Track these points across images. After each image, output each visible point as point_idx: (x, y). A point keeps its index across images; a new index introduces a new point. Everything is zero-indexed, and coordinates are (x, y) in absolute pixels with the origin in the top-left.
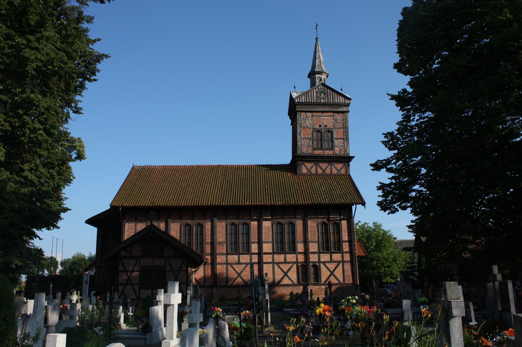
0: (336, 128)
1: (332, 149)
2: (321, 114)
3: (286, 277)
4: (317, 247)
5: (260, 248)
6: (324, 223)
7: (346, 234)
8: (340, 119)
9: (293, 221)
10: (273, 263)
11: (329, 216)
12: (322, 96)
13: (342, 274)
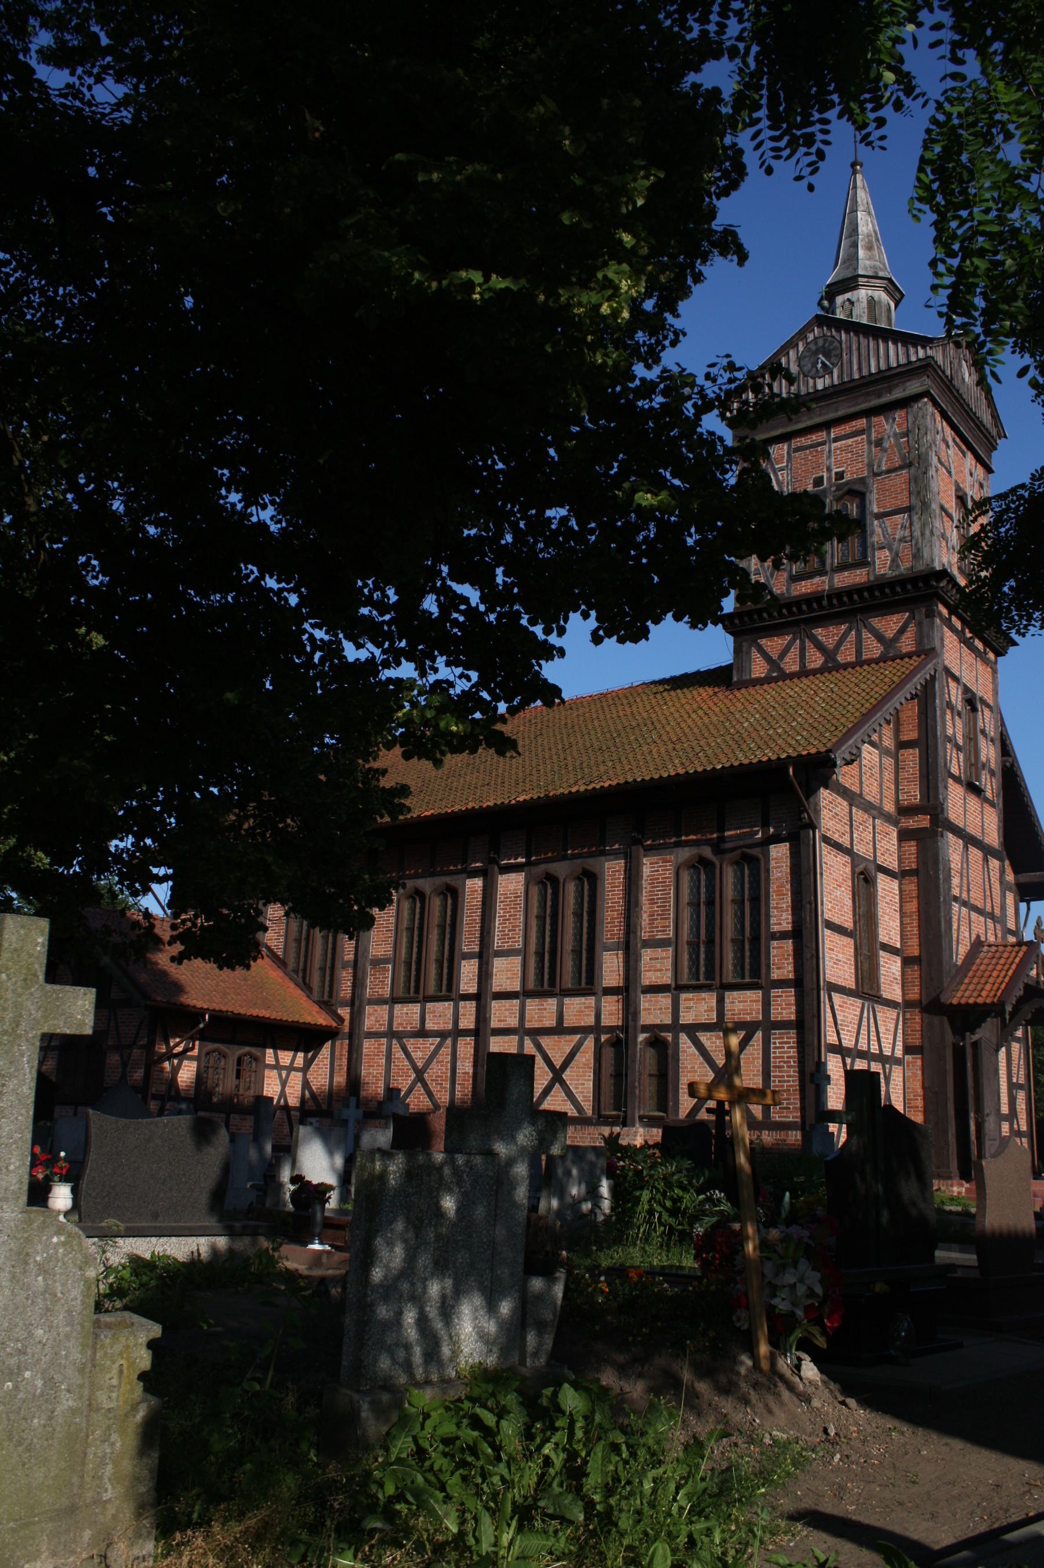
0: (879, 474)
1: (863, 562)
2: (822, 436)
3: (557, 1085)
4: (668, 964)
5: (484, 975)
6: (703, 861)
7: (787, 902)
9: (591, 863)
10: (391, 1034)
11: (724, 832)
12: (819, 365)
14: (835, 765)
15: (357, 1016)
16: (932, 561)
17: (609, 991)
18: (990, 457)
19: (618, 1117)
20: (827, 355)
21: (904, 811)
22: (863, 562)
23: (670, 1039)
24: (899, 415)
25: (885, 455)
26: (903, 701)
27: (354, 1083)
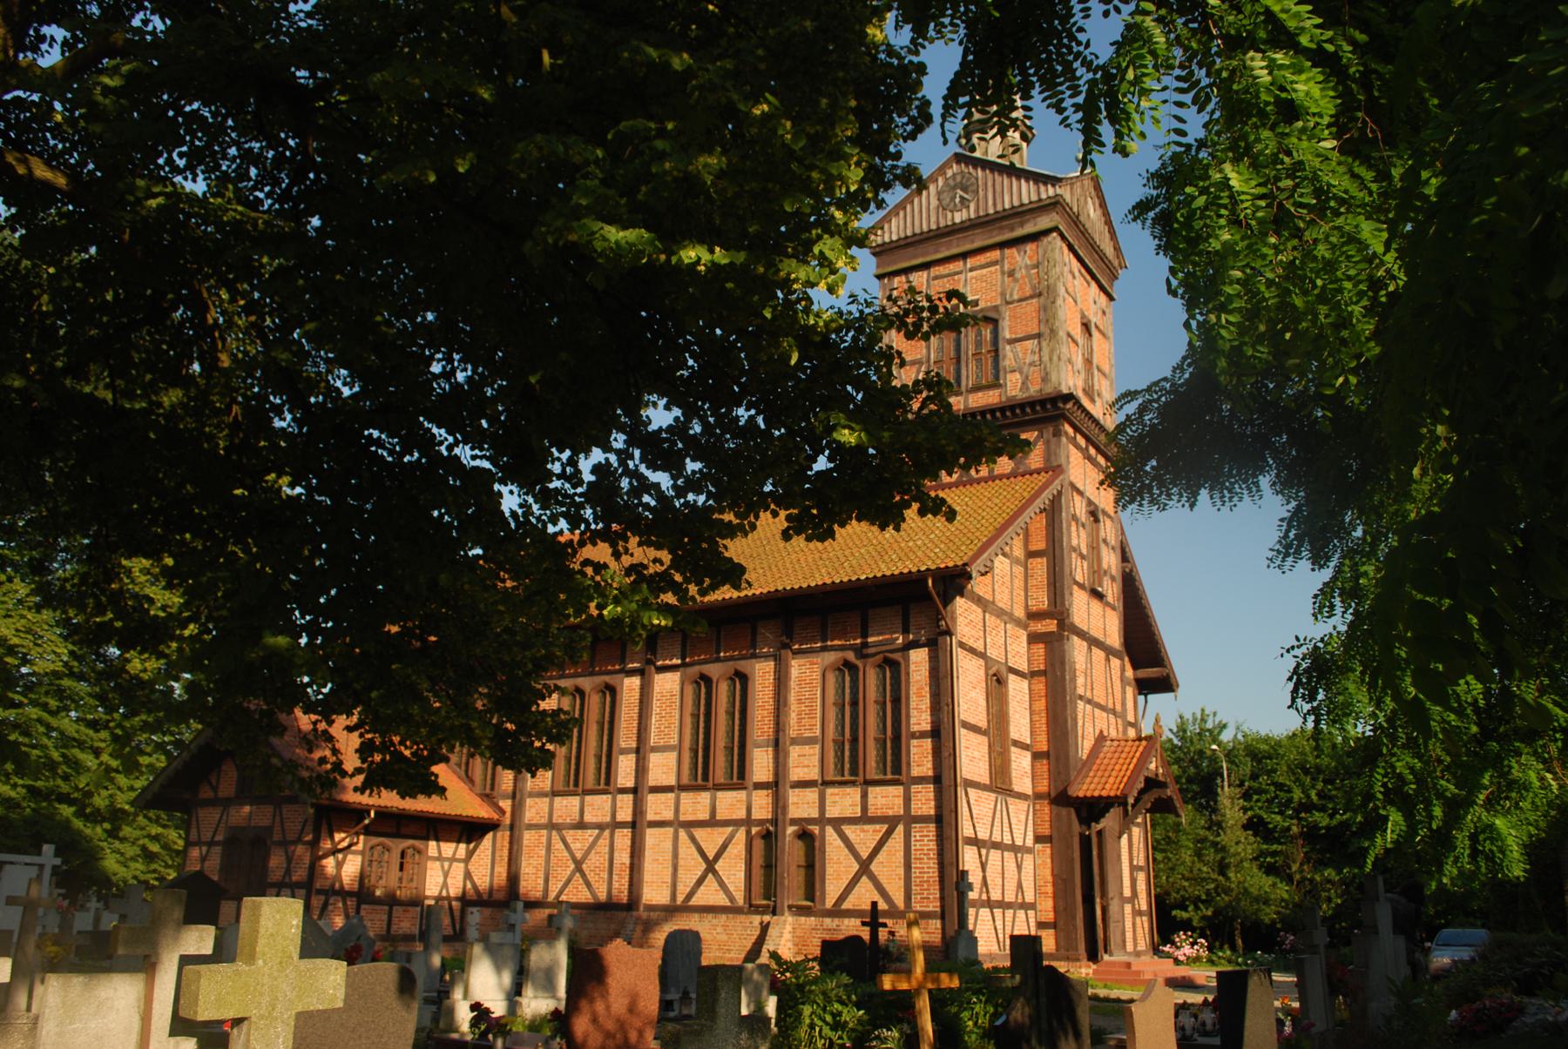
3: (710, 875)
4: (816, 760)
5: (641, 770)
6: (847, 663)
7: (926, 703)
8: (1026, 266)
9: (743, 665)
10: (552, 826)
12: (958, 200)
13: (901, 871)
14: (970, 577)
15: (517, 809)
16: (1060, 384)
17: (759, 786)
18: (1111, 286)
19: (768, 906)
20: (965, 190)
21: (1033, 616)
22: (995, 385)
23: (817, 832)
24: (1030, 247)
26: (1033, 515)
27: (513, 879)
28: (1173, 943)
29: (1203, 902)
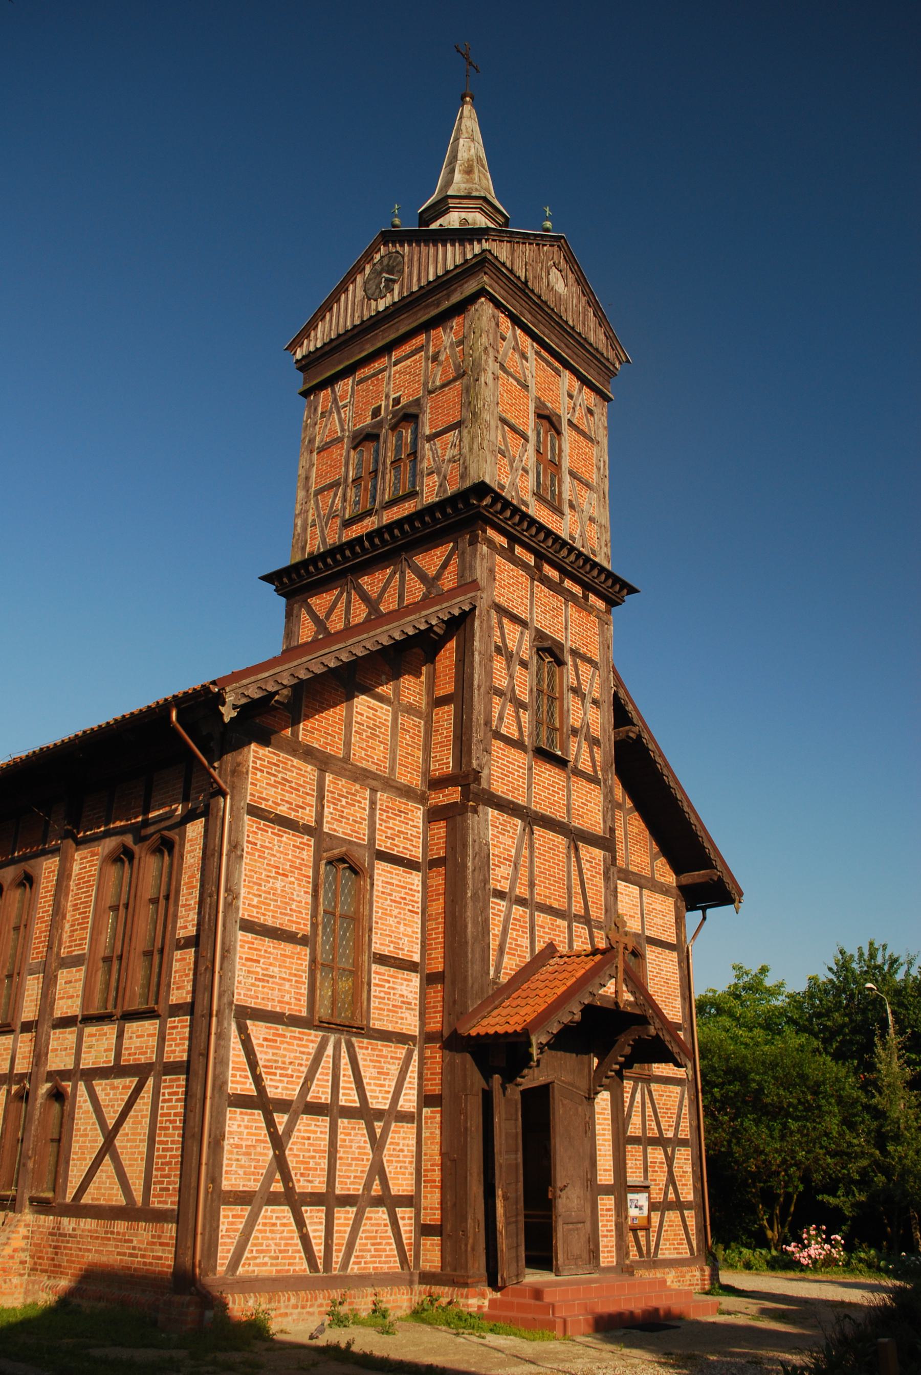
21: (437, 784)
22: (412, 494)
25: (440, 369)
28: (799, 1240)
29: (856, 1183)
